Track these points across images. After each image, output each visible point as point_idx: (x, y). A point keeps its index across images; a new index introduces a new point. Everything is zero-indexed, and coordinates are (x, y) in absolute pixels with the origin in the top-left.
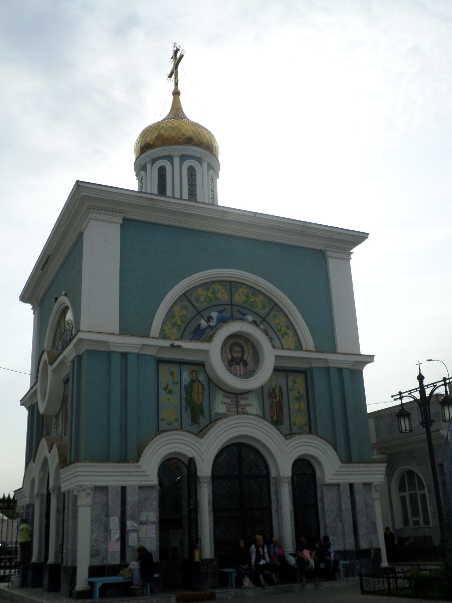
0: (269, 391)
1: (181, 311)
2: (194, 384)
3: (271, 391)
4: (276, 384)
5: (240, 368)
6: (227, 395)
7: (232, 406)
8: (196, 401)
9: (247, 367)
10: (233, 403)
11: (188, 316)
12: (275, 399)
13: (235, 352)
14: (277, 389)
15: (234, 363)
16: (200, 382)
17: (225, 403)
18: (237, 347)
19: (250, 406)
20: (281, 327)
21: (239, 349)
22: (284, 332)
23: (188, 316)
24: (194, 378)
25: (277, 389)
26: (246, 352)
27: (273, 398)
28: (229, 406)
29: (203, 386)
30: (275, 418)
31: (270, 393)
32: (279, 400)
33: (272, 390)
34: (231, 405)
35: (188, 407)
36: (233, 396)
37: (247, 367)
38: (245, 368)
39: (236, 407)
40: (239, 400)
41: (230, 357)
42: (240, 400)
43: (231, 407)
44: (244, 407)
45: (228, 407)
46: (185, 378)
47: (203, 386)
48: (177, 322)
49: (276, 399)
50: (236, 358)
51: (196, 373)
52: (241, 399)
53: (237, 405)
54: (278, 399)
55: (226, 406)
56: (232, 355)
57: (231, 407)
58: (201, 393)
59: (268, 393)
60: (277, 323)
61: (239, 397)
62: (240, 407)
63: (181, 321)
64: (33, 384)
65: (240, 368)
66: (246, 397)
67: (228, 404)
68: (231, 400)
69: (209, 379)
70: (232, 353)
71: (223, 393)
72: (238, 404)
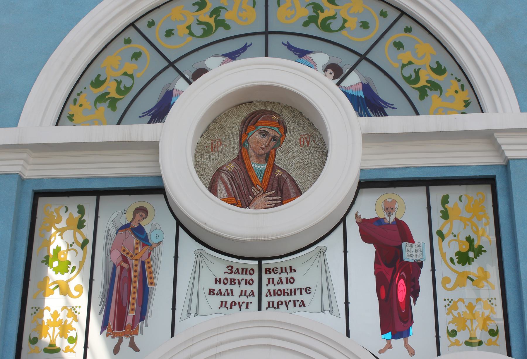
20: (417, 72)
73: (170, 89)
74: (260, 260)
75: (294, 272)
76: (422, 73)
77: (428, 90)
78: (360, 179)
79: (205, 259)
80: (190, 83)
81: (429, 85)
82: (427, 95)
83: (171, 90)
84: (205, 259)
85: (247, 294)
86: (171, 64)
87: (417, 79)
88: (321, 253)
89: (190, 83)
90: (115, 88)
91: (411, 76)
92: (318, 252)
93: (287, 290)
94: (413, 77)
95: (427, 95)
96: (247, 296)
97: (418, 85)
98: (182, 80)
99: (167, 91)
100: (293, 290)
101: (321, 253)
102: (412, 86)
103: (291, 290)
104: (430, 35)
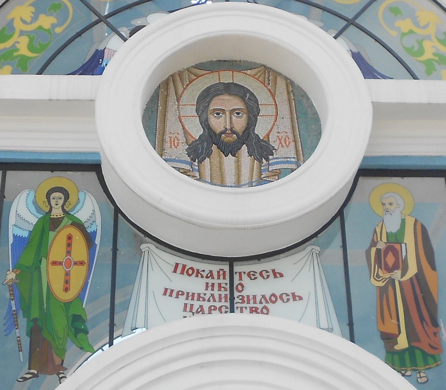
0: (374, 243)
1: (35, 18)
2: (52, 234)
3: (381, 246)
4: (403, 221)
5: (238, 162)
6: (190, 263)
7: (212, 303)
8: (57, 287)
9: (267, 160)
10: (216, 293)
11: (58, 30)
12: (397, 274)
13: (219, 112)
14: (409, 239)
15: (214, 147)
16: (79, 225)
17: (180, 294)
18: (226, 97)
19: (288, 300)
20: (420, 43)
21: (236, 103)
22: (434, 54)
23: (58, 30)
24: (57, 212)
25: (409, 239)
26: (266, 110)
27: (390, 270)
28: (197, 304)
29: (89, 238)
30: (402, 342)
31: (378, 251)
32: (420, 276)
33: (384, 239)
34: (204, 300)
35: (21, 313)
36: (215, 267)
37: (267, 160)
38: (260, 162)
39: (228, 304)
40: (241, 279)
41: (197, 131)
42: (246, 280)
43: (206, 305)
44: (264, 304)
45: (192, 306)
46: (18, 215)
47: (89, 238)
48: (18, 50)
49: (404, 273)
50: (222, 133)
51: (67, 196)
52: (251, 275)
53: (232, 299)
54: (412, 270)
55: (186, 305)
56: (205, 124)
57: (206, 305)
58: (82, 263)
59: (368, 253)
60: (406, 30)
61: (238, 268)
62: (245, 305)
63: (31, 47)
64: (347, 329)
65: (238, 162)
66: (274, 271)
67: (190, 296)
68: (205, 280)
69: (117, 211)
70: (207, 120)
71: (173, 259)
72: (236, 294)
73: (101, 48)
74: (231, 261)
75: (280, 277)
76: (427, 45)
77: (435, 63)
78: (365, 158)
79: (153, 254)
80: (125, 40)
81: (437, 58)
82: (435, 70)
83: (101, 50)
84: (153, 254)
85: (194, 311)
86: (101, 19)
87: (421, 52)
88: (312, 254)
89: (125, 40)
90: (27, 44)
91: (413, 47)
92: (309, 254)
93: (204, 295)
94: (416, 48)
95: (435, 70)
96: (193, 313)
97: (424, 58)
98: (116, 38)
99: (97, 50)
100: (251, 297)
101: (312, 254)
102: (416, 58)
103: (221, 296)
104: (262, 260)
